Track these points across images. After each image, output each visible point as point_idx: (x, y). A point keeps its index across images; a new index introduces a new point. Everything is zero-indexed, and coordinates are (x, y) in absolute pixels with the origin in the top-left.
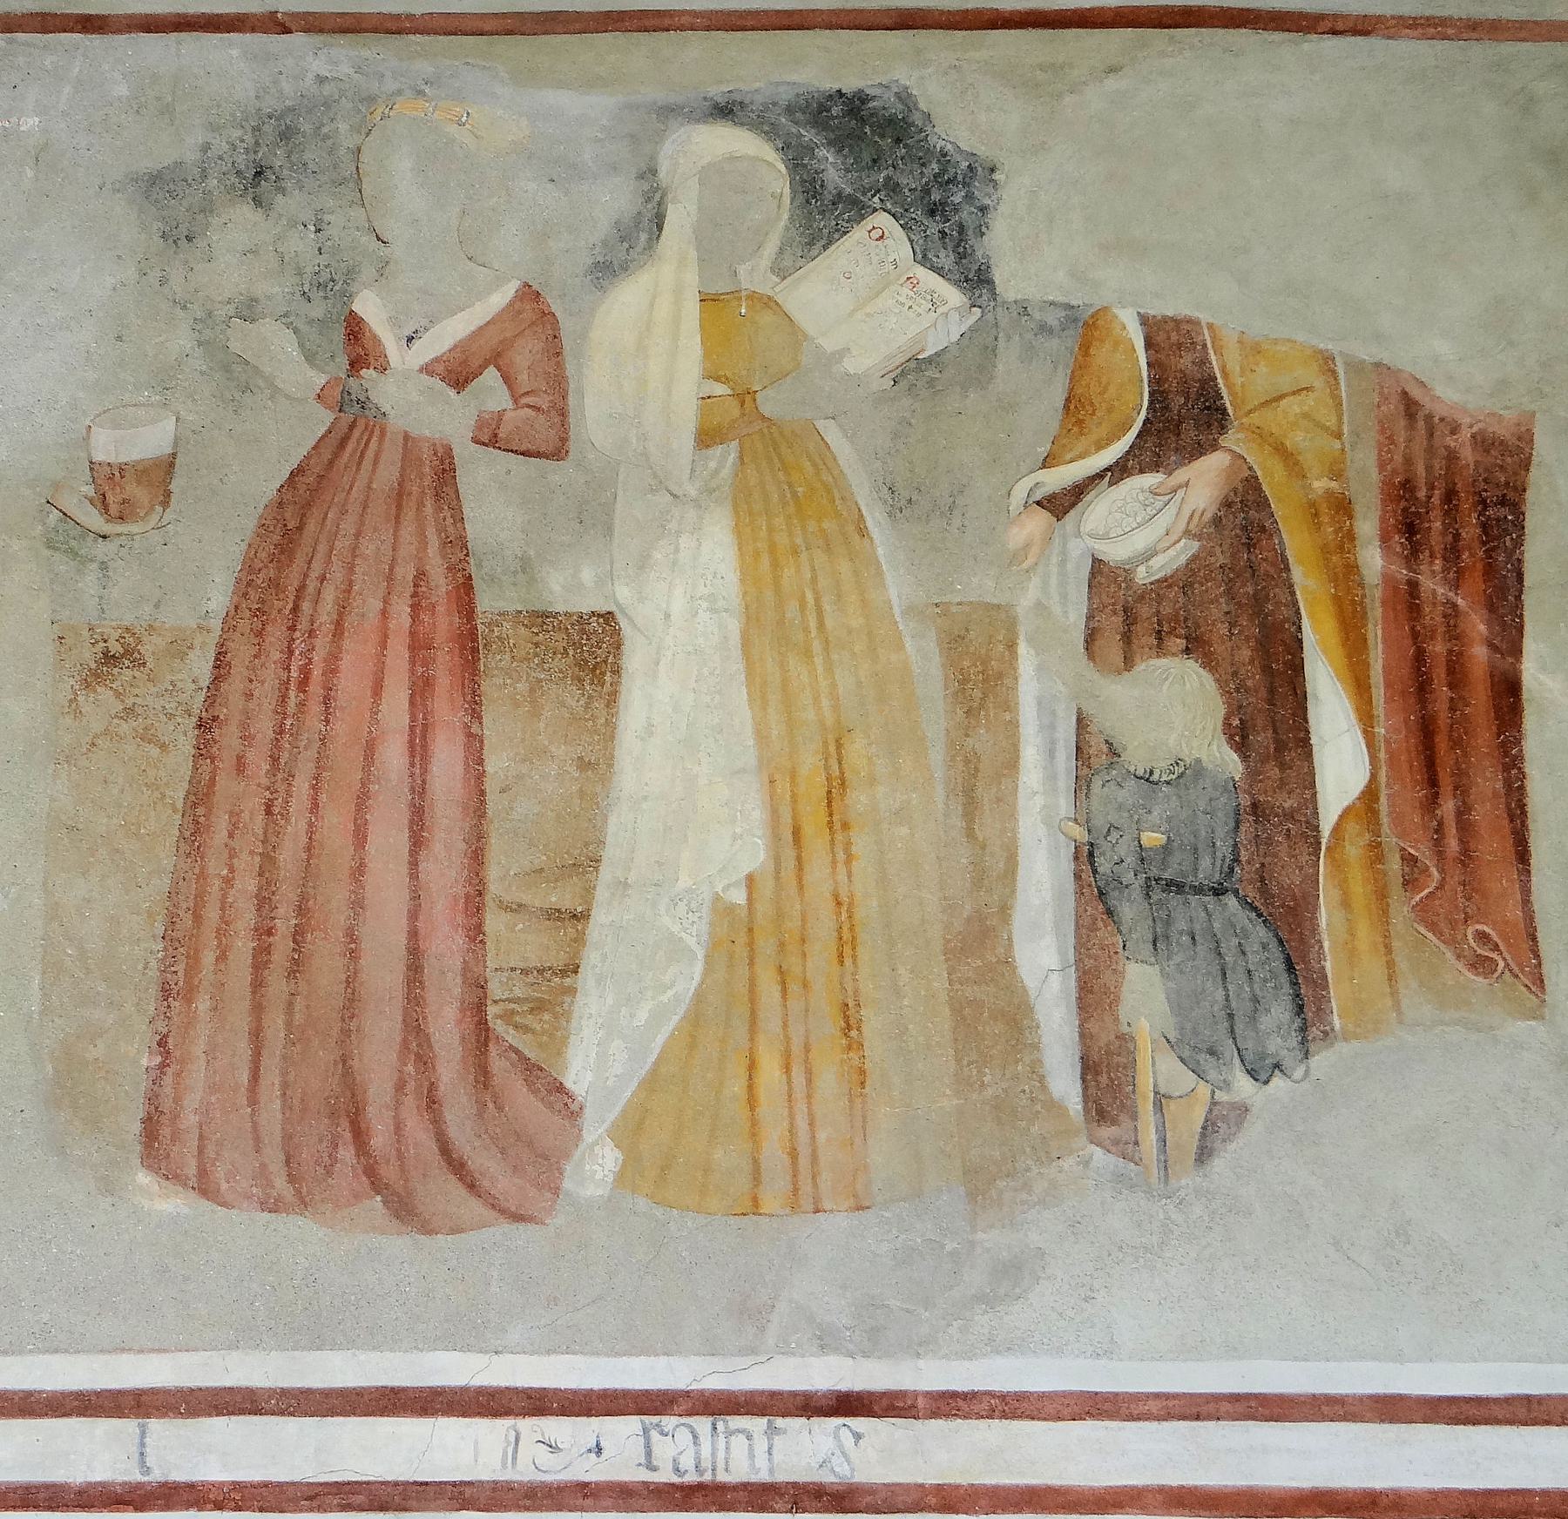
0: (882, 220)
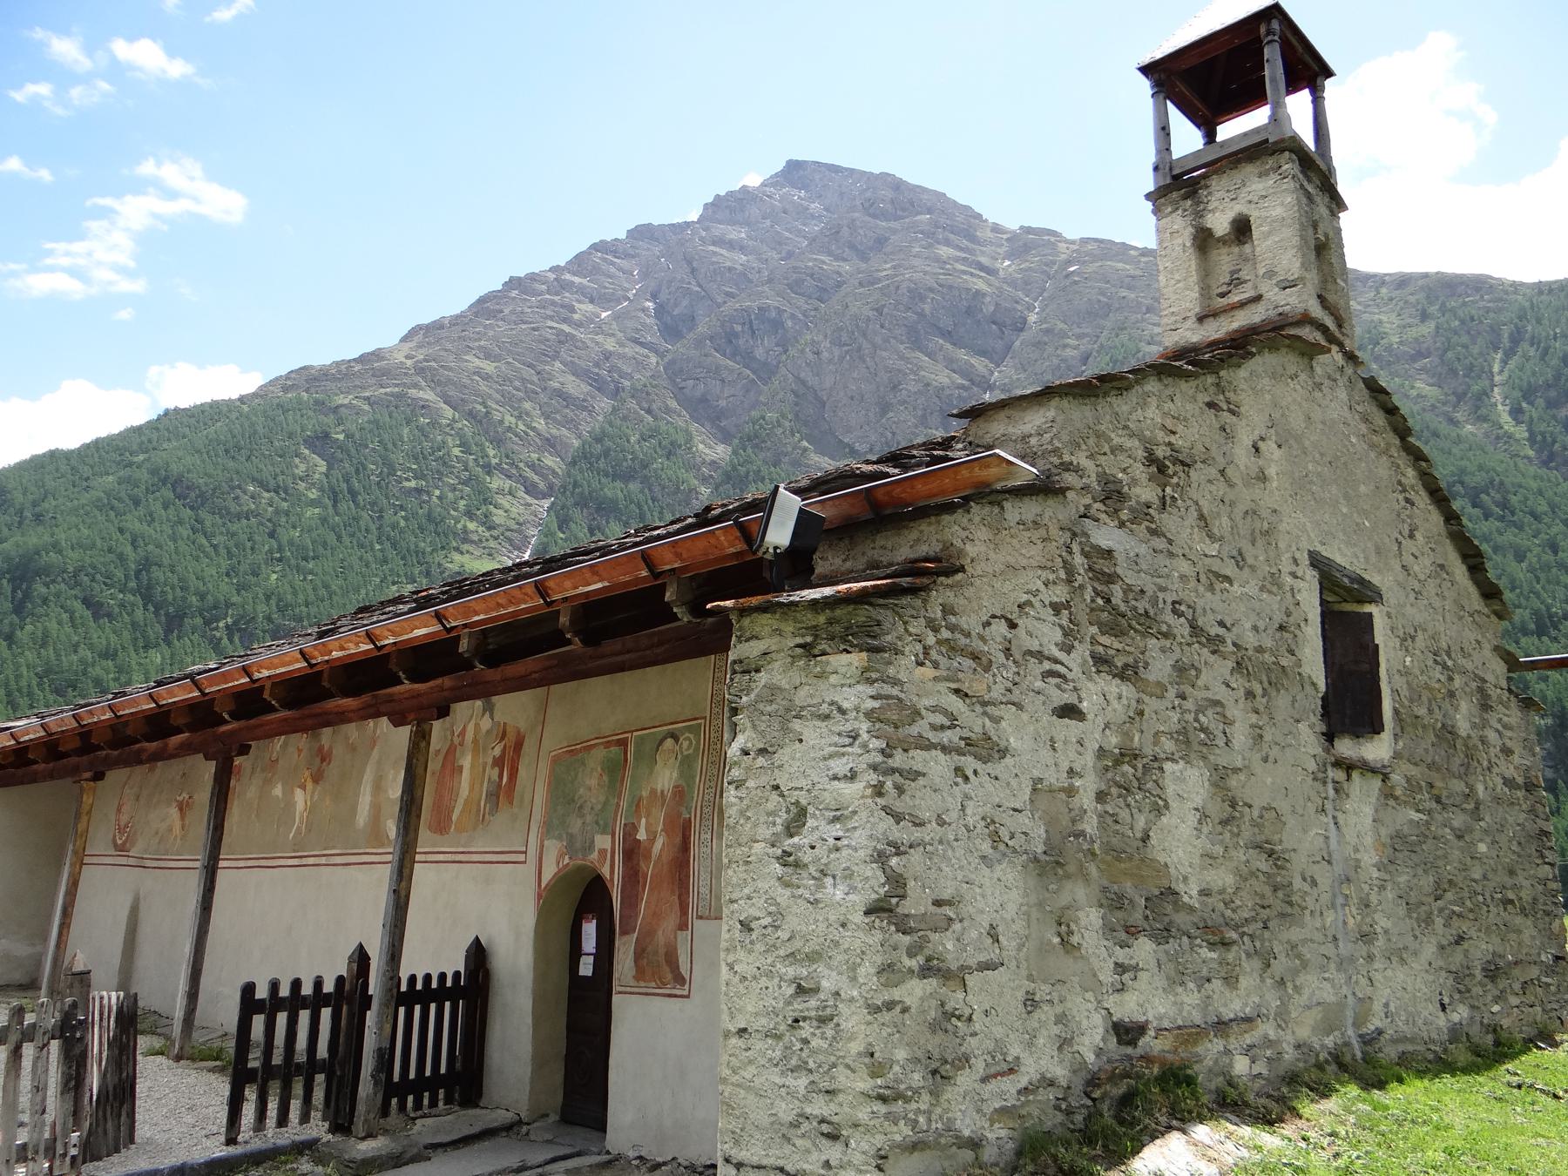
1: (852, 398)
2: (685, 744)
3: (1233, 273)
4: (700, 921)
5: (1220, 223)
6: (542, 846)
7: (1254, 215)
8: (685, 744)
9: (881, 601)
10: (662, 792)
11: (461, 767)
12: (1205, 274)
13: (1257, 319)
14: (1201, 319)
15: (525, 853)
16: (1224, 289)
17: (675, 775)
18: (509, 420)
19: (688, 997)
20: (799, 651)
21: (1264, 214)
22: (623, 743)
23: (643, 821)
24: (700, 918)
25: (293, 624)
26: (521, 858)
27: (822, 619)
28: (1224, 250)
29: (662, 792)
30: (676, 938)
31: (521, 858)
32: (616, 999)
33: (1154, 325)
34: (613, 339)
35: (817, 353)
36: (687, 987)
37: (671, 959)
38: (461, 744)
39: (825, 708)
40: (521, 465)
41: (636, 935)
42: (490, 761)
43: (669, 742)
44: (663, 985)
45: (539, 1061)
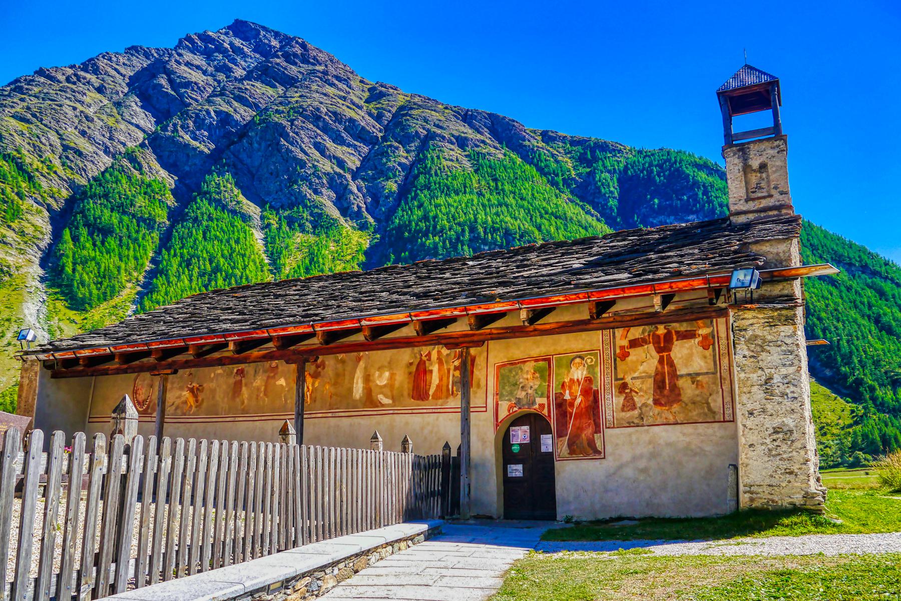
1: (271, 174)
2: (589, 361)
3: (757, 184)
5: (755, 163)
6: (497, 405)
7: (769, 163)
8: (589, 361)
9: (749, 306)
10: (578, 380)
11: (431, 371)
12: (747, 183)
13: (771, 204)
14: (747, 201)
16: (754, 190)
17: (585, 373)
18: (37, 164)
19: (604, 458)
20: (767, 324)
21: (773, 163)
22: (549, 361)
23: (567, 392)
24: (606, 428)
25: (330, 303)
26: (484, 409)
27: (776, 314)
28: (754, 174)
29: (578, 380)
30: (593, 437)
31: (484, 409)
32: (556, 463)
33: (451, 150)
34: (113, 119)
35: (251, 144)
36: (603, 454)
37: (591, 444)
38: (429, 360)
39: (779, 343)
40: (45, 195)
42: (452, 368)
43: (578, 360)
44: (588, 455)
45: (498, 495)
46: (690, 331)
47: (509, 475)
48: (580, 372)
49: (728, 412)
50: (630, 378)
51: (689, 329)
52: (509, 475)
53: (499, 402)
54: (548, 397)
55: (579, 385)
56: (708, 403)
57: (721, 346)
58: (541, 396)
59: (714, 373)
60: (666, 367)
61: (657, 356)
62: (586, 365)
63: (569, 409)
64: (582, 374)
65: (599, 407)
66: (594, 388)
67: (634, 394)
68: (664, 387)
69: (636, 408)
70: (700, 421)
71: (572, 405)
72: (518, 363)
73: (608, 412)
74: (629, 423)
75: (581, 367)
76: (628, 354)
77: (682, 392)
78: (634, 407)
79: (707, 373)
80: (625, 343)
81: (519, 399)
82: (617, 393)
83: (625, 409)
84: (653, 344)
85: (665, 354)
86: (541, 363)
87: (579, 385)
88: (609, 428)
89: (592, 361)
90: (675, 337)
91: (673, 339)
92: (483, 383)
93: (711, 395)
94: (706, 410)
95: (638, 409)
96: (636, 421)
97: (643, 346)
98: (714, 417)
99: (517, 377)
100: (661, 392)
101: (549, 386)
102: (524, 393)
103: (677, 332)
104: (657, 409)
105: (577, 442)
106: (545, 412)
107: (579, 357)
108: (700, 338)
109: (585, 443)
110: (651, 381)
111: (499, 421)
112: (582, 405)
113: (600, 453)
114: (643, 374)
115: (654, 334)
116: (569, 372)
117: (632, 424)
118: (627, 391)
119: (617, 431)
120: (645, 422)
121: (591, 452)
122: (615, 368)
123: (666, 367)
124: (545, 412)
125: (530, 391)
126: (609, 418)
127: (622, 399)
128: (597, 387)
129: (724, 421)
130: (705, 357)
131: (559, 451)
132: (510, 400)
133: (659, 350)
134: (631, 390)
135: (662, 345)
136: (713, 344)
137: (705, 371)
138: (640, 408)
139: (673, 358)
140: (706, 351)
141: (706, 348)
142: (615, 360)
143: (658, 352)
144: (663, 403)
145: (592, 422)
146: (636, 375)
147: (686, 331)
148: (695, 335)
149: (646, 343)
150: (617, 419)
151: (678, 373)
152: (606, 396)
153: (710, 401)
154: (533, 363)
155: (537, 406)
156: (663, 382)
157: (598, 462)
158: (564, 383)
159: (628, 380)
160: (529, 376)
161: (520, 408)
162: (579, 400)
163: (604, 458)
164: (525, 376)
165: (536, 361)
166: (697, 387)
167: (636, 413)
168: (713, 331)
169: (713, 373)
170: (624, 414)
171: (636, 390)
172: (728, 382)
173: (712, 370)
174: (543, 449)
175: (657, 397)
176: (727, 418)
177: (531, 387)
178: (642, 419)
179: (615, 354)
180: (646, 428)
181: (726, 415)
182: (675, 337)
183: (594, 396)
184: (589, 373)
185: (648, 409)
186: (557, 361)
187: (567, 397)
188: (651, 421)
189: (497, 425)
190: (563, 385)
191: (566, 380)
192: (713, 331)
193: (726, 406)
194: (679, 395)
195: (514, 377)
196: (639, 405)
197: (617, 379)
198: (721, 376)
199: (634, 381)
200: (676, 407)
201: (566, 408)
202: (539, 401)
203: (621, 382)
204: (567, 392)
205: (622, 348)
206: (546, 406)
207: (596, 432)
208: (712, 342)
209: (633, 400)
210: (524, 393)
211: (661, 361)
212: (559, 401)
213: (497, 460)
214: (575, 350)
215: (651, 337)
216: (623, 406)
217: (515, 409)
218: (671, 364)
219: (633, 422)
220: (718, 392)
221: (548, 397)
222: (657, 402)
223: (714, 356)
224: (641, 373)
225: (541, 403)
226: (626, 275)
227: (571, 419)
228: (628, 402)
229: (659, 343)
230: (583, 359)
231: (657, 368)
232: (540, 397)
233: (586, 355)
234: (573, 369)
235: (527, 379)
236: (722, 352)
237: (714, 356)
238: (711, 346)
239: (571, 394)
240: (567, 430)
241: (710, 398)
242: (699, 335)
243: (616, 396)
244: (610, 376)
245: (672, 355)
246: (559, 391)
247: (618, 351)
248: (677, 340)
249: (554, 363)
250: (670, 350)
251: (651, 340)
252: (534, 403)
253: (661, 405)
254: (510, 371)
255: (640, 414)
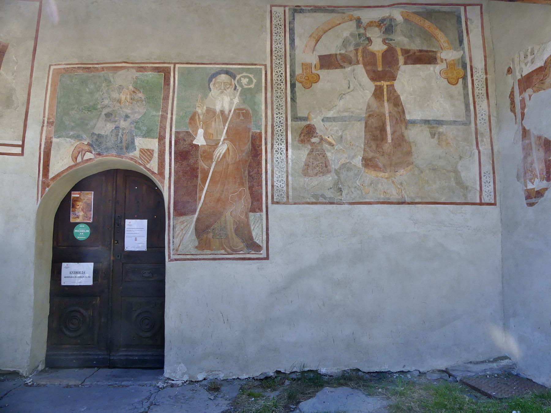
0: (64, 265)
2: (245, 81)
4: (275, 206)
8: (245, 81)
10: (222, 112)
15: (22, 146)
17: (236, 101)
19: (267, 258)
22: (166, 73)
23: (201, 131)
24: (273, 202)
29: (222, 112)
30: (247, 217)
31: (18, 150)
41: (196, 216)
44: (235, 251)
46: (427, 51)
47: (65, 281)
48: (227, 99)
49: (488, 188)
50: (320, 118)
51: (425, 48)
52: (65, 281)
53: (54, 140)
54: (161, 139)
55: (225, 121)
56: (456, 172)
57: (475, 82)
58: (148, 134)
59: (466, 124)
60: (386, 104)
61: (370, 86)
62: (239, 88)
63: (202, 164)
64: (231, 103)
65: (260, 163)
66: (255, 130)
67: (326, 146)
68: (383, 138)
69: (329, 172)
70: (443, 200)
71: (208, 156)
72: (103, 69)
73: (277, 174)
74: (315, 196)
75: (230, 90)
76: (317, 78)
77: (414, 149)
78: (325, 168)
79: (455, 122)
80: (313, 59)
81: (99, 136)
82: (296, 143)
83: (310, 172)
84: (365, 65)
85: (385, 84)
86: (150, 75)
87: (225, 121)
88: (278, 203)
89: (250, 82)
90: (401, 59)
91: (397, 61)
92: (20, 97)
93: (461, 158)
94: (453, 183)
95: (333, 173)
96: (329, 194)
97: (342, 67)
98: (465, 196)
99: (97, 95)
100: (377, 146)
101: (164, 118)
102: (110, 127)
103: (406, 52)
104: (370, 175)
105: (216, 226)
106: (154, 165)
107: (227, 72)
108: (444, 66)
109: (231, 228)
110: (360, 127)
111: (51, 175)
112: (229, 159)
113: (258, 248)
114: (346, 114)
115: (365, 51)
116: (206, 96)
117: (321, 200)
118: (314, 140)
119: (293, 209)
120: (344, 197)
121: (242, 245)
122: (293, 99)
123: (386, 104)
124: (154, 165)
125: (123, 124)
126: (280, 184)
127: (304, 153)
128: (259, 127)
129: (481, 204)
130: (451, 97)
131: (177, 241)
132: (78, 137)
133: (375, 76)
134: (322, 139)
135: (380, 69)
136: (465, 78)
137: (452, 119)
138: (337, 172)
139: (399, 92)
140: (453, 87)
141: (452, 82)
142: (293, 86)
143: (373, 79)
144: (380, 165)
145: (247, 191)
146: (331, 114)
147: (421, 51)
148: (435, 59)
149: (350, 63)
150: (294, 189)
151: (408, 117)
152: (276, 147)
153: (459, 168)
154: (134, 74)
155: (136, 153)
156: (383, 129)
157: (254, 265)
158: (195, 114)
159: (316, 121)
160: (123, 97)
161: (99, 154)
162: (222, 149)
163: (267, 258)
164: (115, 95)
165: (141, 69)
166: (439, 144)
167: (329, 179)
168: (463, 57)
169: (464, 124)
170: (307, 179)
171: (330, 140)
172: (487, 140)
173: (463, 119)
174: (89, 282)
175: (371, 154)
176: (486, 199)
177: (127, 116)
178: (340, 190)
179: (292, 75)
180: (346, 207)
181: (484, 193)
182: (401, 59)
183: (253, 145)
184: (244, 100)
185: (351, 174)
186: (181, 74)
187: (200, 140)
188: (355, 196)
189: (45, 185)
190: (193, 119)
191: (199, 111)
192: (463, 57)
193: (483, 178)
194: (409, 153)
195: (91, 93)
196: (334, 166)
197: (295, 118)
198: (476, 129)
199: (327, 124)
200: (403, 174)
201: (196, 162)
202: (141, 143)
203: (304, 123)
204: (201, 131)
205: (306, 66)
206: (156, 155)
207: (253, 210)
208: (462, 73)
209: (324, 156)
210: (110, 127)
211: (378, 94)
212: (183, 146)
213: (39, 253)
214: (220, 60)
215: (360, 54)
216: (307, 165)
217: (88, 156)
218: (396, 102)
219: (323, 196)
220: (472, 155)
221: (161, 139)
222: (368, 163)
223: (466, 96)
224: (339, 112)
225: (145, 147)
226: (219, 161)
227: (204, 182)
228: (315, 159)
229: (375, 64)
230: (234, 77)
231: (369, 106)
232: (145, 136)
233: (241, 71)
234: (214, 92)
235: (119, 101)
236: (476, 91)
237: (466, 96)
238: (461, 81)
239: (206, 136)
240: (196, 201)
241: (460, 164)
242: (442, 61)
243: (293, 147)
244: (283, 111)
245: (397, 85)
246: (185, 129)
247: (298, 71)
248: (406, 63)
249: (175, 79)
250: (394, 78)
251: (361, 59)
252: (131, 146)
253: (376, 167)
254: (84, 82)
255: (336, 183)
